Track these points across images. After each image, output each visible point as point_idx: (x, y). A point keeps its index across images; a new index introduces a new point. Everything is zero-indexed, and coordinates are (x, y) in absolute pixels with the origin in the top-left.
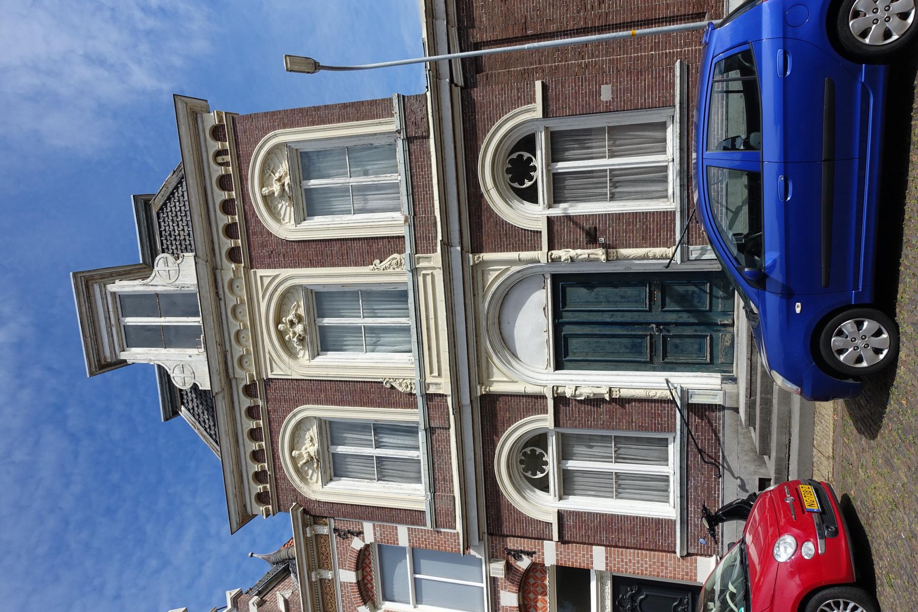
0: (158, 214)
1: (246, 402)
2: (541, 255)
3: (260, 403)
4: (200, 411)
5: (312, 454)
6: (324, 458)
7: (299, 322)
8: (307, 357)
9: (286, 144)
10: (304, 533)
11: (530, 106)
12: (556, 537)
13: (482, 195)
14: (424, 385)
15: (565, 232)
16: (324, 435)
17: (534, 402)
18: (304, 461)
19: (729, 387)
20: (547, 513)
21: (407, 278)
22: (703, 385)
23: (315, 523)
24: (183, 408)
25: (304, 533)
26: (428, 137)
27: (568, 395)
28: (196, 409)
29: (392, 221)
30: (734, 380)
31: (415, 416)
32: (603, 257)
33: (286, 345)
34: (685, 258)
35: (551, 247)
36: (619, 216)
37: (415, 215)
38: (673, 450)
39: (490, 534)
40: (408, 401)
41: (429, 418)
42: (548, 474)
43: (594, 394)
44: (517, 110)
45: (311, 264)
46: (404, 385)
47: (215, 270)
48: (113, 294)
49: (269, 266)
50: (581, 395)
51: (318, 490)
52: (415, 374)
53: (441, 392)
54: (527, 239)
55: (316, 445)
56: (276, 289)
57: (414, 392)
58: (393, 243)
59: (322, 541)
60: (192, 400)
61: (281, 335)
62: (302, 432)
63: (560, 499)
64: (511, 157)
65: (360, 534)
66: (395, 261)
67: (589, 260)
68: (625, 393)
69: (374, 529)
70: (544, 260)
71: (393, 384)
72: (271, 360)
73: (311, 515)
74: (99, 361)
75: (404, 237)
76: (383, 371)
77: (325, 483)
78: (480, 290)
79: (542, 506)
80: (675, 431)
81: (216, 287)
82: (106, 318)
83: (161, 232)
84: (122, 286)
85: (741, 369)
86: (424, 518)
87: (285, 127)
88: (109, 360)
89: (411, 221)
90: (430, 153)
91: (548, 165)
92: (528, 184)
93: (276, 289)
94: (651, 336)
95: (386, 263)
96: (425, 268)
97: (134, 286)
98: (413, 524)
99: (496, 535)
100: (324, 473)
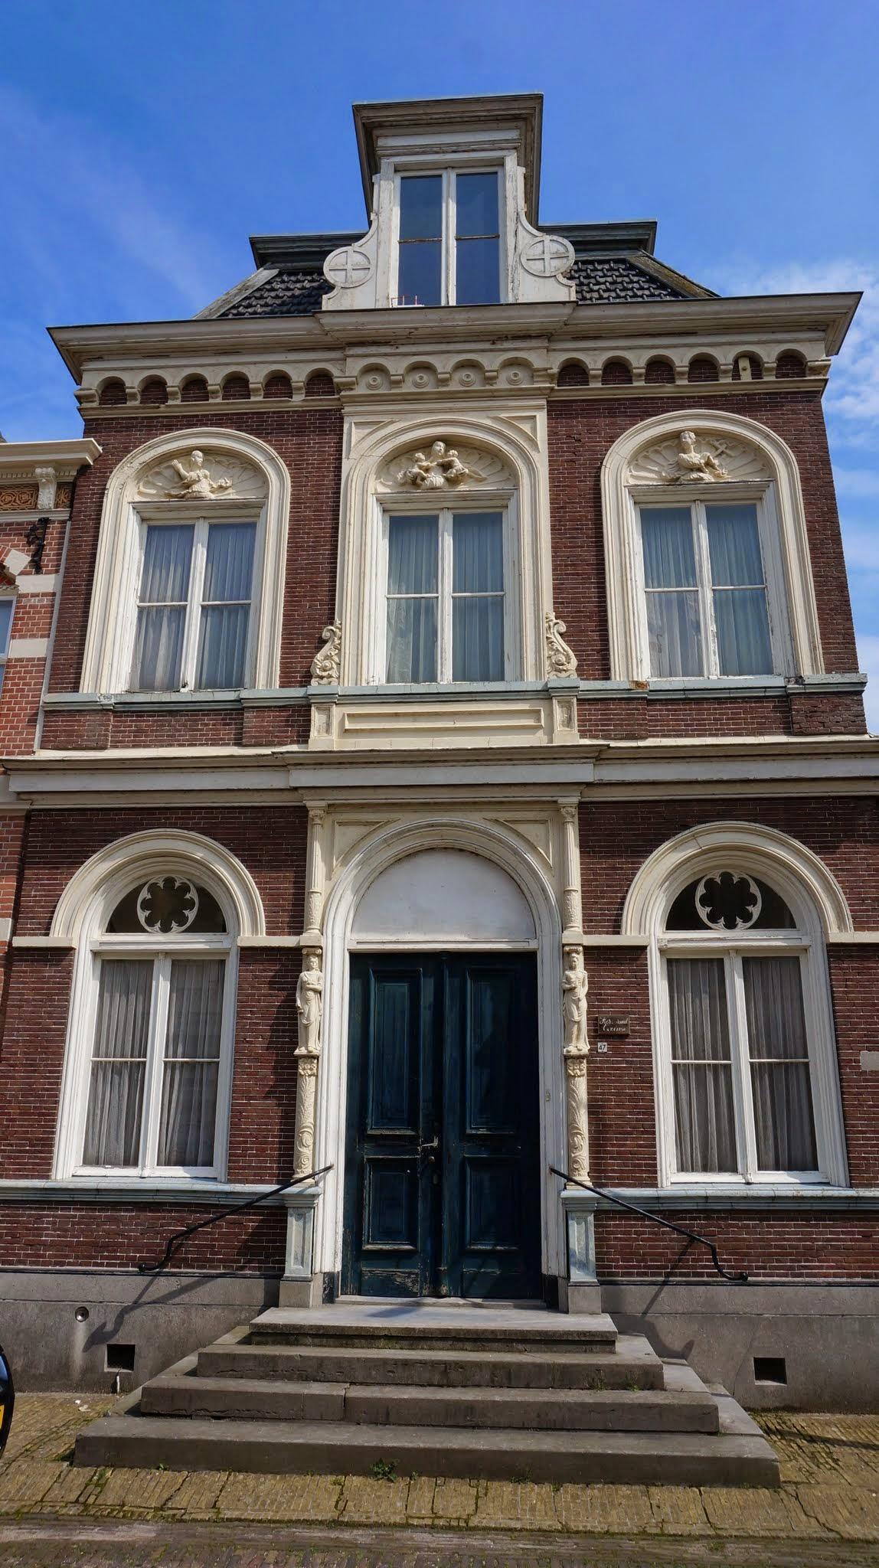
0: (623, 261)
1: (299, 375)
2: (576, 933)
3: (298, 399)
4: (269, 301)
5: (195, 488)
6: (187, 508)
7: (447, 479)
8: (381, 489)
9: (773, 479)
10: (44, 464)
11: (849, 922)
12: (19, 942)
13: (686, 827)
14: (328, 701)
15: (615, 978)
16: (231, 512)
17: (293, 911)
18: (183, 471)
19: (317, 1289)
20: (69, 927)
21: (531, 681)
22: (322, 1240)
23: (60, 486)
24: (275, 272)
25: (44, 464)
26: (788, 732)
27: (305, 976)
28: (273, 294)
29: (636, 660)
30: (330, 1298)
31: (265, 680)
32: (574, 1051)
33: (407, 451)
34: (571, 1209)
35: (590, 952)
36: (647, 1081)
37: (650, 702)
38: (177, 1177)
39: (29, 816)
40: (296, 670)
41: (262, 708)
42: (144, 931)
43: (306, 1027)
44: (842, 897)
45: (557, 510)
46: (327, 663)
47: (548, 336)
48: (501, 163)
49: (552, 433)
50: (306, 1001)
51: (124, 497)
52: (347, 686)
53: (313, 733)
54: (605, 909)
55: (213, 496)
56: (510, 441)
57: (314, 682)
58: (595, 654)
59: (25, 497)
60: (288, 289)
61: (426, 445)
62: (237, 471)
63: (96, 954)
64: (752, 883)
65: (36, 566)
66: (563, 659)
67: (567, 1023)
68: (308, 1087)
69: (44, 595)
70: (568, 937)
71: (327, 646)
72: (379, 425)
73: (76, 478)
74: (381, 125)
75: (608, 679)
76: (354, 626)
77: (137, 508)
78: (509, 815)
79: (81, 919)
80: (230, 1181)
81: (517, 337)
82: (458, 144)
83: (591, 262)
84: (514, 175)
85: (355, 1312)
86: (64, 690)
87: (805, 480)
88: (381, 142)
89: (639, 693)
90: (762, 734)
91: (737, 950)
92: (703, 912)
93: (510, 441)
94: (413, 1140)
95: (560, 643)
96: (550, 715)
97: (515, 198)
98: (54, 667)
99: (26, 827)
100: (158, 507)
